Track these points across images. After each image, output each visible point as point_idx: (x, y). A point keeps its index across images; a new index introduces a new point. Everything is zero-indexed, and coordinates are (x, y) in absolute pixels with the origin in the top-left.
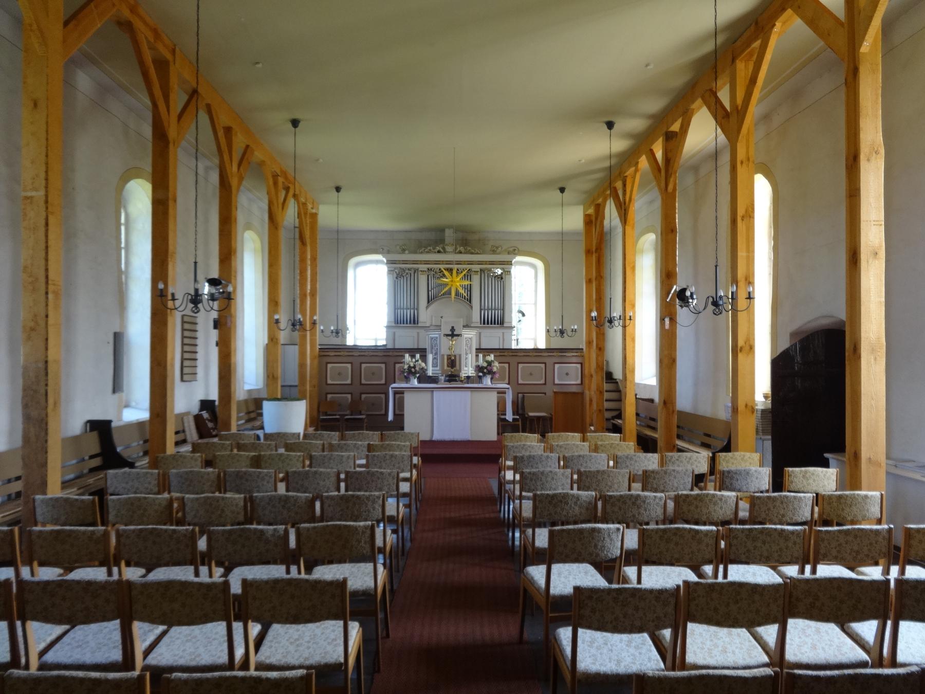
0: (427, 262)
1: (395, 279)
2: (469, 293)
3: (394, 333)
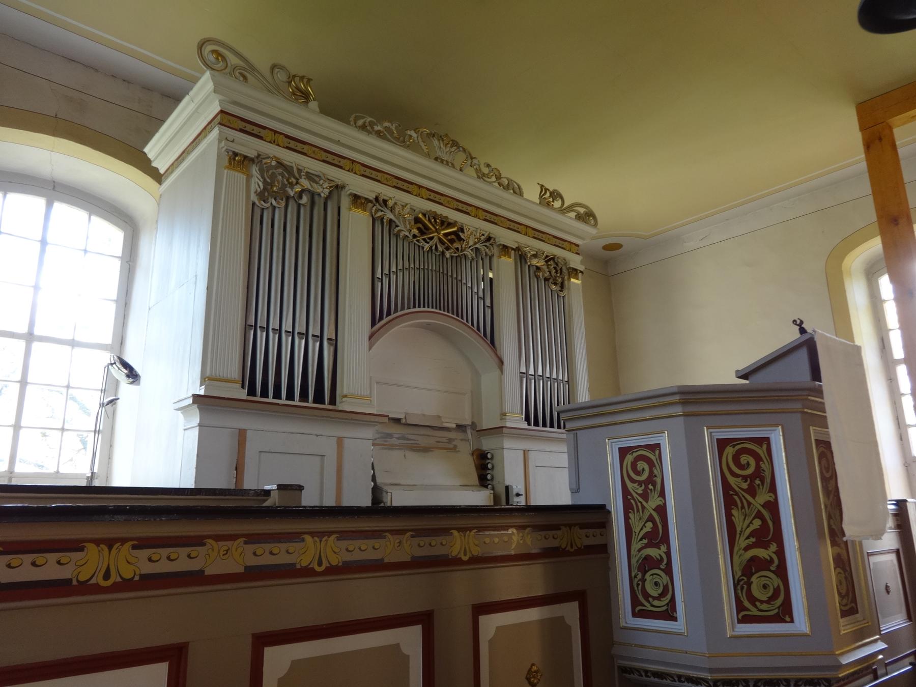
0: (371, 173)
1: (254, 198)
2: (488, 311)
3: (242, 436)
